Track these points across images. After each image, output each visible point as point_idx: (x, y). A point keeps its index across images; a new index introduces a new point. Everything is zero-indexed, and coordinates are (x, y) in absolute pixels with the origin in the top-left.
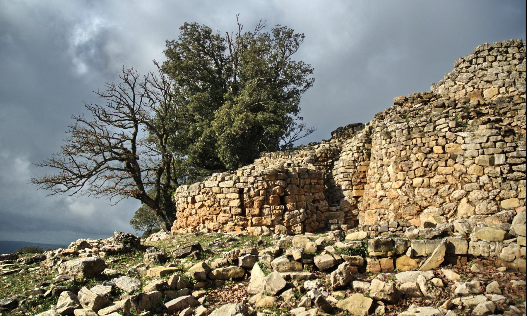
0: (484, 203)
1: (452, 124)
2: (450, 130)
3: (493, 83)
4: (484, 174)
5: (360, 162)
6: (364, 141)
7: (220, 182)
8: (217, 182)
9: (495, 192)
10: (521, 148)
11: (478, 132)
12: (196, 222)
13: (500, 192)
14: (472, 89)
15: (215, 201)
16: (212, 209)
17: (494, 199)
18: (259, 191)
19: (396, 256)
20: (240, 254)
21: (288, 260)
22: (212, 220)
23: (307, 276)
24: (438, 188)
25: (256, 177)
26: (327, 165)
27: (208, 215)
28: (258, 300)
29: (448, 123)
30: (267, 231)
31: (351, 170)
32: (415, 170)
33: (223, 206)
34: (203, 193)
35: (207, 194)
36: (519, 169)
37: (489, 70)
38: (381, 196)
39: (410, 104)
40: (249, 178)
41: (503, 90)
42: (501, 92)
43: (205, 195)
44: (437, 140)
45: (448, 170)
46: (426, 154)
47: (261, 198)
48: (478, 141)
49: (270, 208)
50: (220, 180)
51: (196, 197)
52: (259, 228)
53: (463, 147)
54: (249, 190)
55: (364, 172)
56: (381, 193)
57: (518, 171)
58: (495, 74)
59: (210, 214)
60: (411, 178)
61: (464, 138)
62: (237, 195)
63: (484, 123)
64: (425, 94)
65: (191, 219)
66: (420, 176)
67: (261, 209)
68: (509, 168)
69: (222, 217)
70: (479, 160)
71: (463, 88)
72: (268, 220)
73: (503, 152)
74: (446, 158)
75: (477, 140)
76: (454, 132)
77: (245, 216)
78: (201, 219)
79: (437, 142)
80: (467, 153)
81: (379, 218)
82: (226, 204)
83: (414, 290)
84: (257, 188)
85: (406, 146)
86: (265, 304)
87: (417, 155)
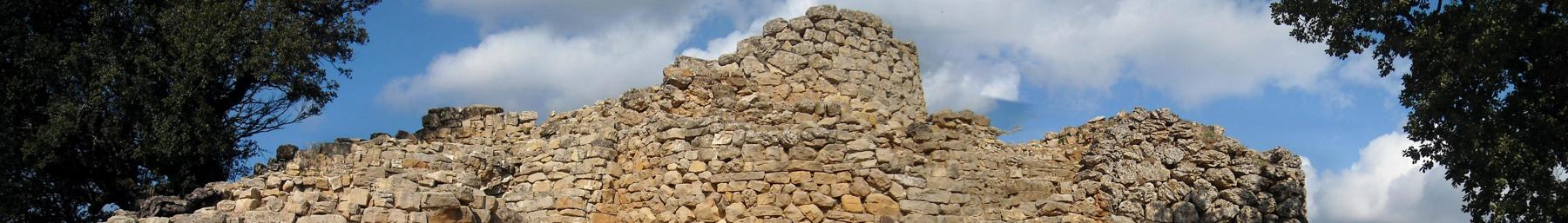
3: (842, 86)
48: (932, 197)
61: (906, 187)
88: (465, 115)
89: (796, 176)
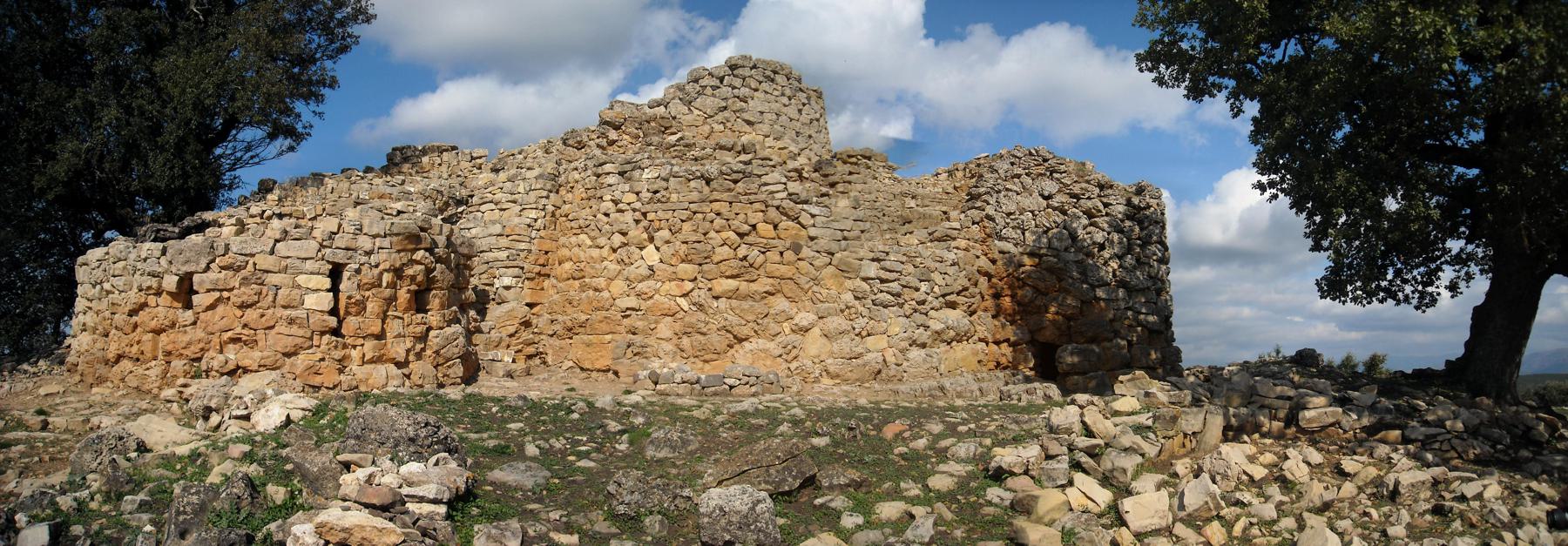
6: (549, 186)
16: (251, 315)
27: (239, 330)
31: (523, 246)
33: (284, 307)
34: (223, 268)
51: (196, 278)
59: (245, 326)
61: (813, 216)
62: (326, 283)
84: (377, 266)
88: (424, 152)
89: (716, 206)
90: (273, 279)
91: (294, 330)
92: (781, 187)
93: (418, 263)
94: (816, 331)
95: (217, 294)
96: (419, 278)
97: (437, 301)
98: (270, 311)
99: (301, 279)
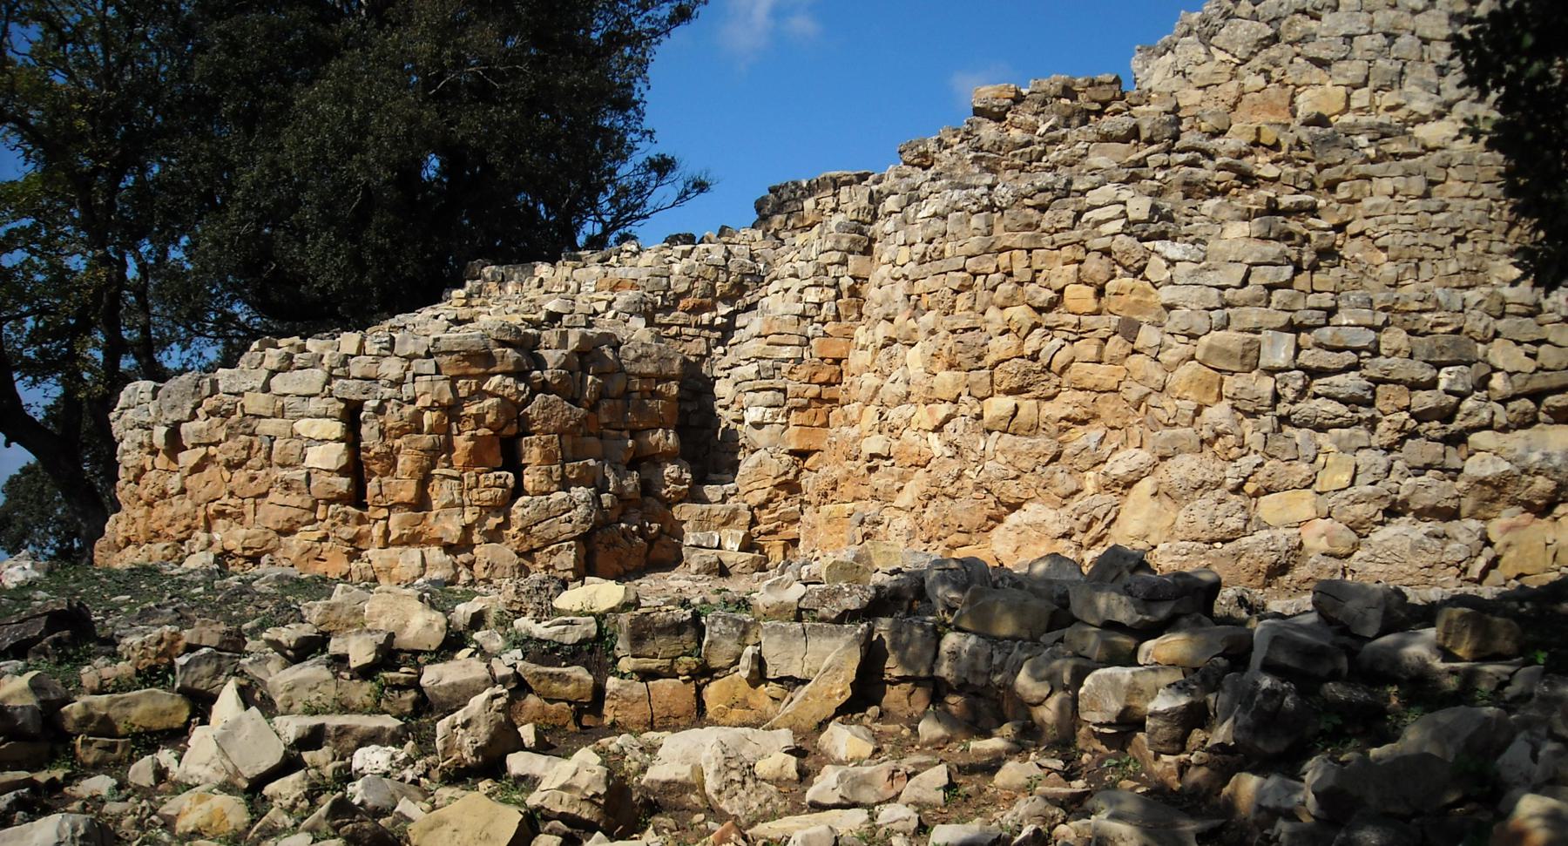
0: (1206, 502)
1: (1139, 207)
2: (1128, 230)
3: (1335, 67)
4: (1220, 397)
5: (824, 323)
6: (845, 244)
7: (273, 373)
8: (263, 374)
9: (1247, 464)
10: (1350, 315)
11: (1221, 245)
12: (180, 526)
13: (1261, 465)
14: (1260, 81)
15: (251, 446)
16: (240, 476)
17: (1238, 489)
18: (419, 414)
19: (704, 673)
20: (181, 644)
21: (327, 674)
22: (239, 517)
23: (383, 729)
24: (1065, 437)
25: (410, 358)
26: (711, 326)
27: (225, 499)
28: (186, 807)
29: (1124, 203)
30: (443, 564)
31: (786, 352)
32: (993, 367)
33: (283, 466)
34: (210, 413)
35: (228, 414)
36: (1332, 391)
37: (1327, 17)
38: (873, 456)
39: (1031, 119)
40: (385, 362)
41: (1361, 98)
42: (1354, 104)
43: (216, 420)
44: (1081, 262)
45: (1103, 374)
46: (1039, 310)
47: (426, 440)
48: (1213, 278)
49: (461, 479)
50: (275, 366)
51: (184, 428)
52: (414, 553)
53: (1166, 294)
54: (380, 410)
55: (837, 361)
56: (875, 444)
57: (1328, 396)
58: (1345, 36)
59: (232, 494)
60: (980, 394)
61: (1172, 263)
62: (336, 428)
63: (1247, 216)
64: (1092, 84)
65: (163, 511)
66: (1009, 392)
67: (424, 481)
68: (1300, 382)
69: (278, 507)
70: (1210, 348)
71: (1234, 75)
72: (450, 526)
73: (1294, 328)
74: (1102, 333)
75: (1210, 275)
76: (1141, 240)
77: (365, 507)
78: (201, 513)
79: (1079, 270)
80: (1177, 319)
81: (859, 532)
82: (293, 460)
83: (684, 787)
84: (413, 401)
85: (975, 275)
86: (206, 820)
87: (1008, 312)
88: (811, 190)
89: (1004, 259)
90: (267, 426)
91: (294, 499)
92: (1115, 210)
93: (492, 394)
94: (1146, 485)
95: (202, 450)
96: (490, 418)
97: (536, 451)
98: (263, 472)
99: (302, 426)
